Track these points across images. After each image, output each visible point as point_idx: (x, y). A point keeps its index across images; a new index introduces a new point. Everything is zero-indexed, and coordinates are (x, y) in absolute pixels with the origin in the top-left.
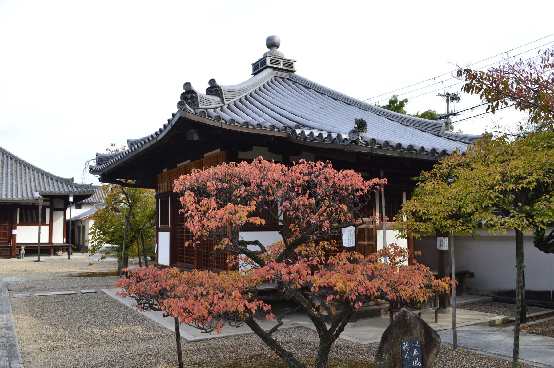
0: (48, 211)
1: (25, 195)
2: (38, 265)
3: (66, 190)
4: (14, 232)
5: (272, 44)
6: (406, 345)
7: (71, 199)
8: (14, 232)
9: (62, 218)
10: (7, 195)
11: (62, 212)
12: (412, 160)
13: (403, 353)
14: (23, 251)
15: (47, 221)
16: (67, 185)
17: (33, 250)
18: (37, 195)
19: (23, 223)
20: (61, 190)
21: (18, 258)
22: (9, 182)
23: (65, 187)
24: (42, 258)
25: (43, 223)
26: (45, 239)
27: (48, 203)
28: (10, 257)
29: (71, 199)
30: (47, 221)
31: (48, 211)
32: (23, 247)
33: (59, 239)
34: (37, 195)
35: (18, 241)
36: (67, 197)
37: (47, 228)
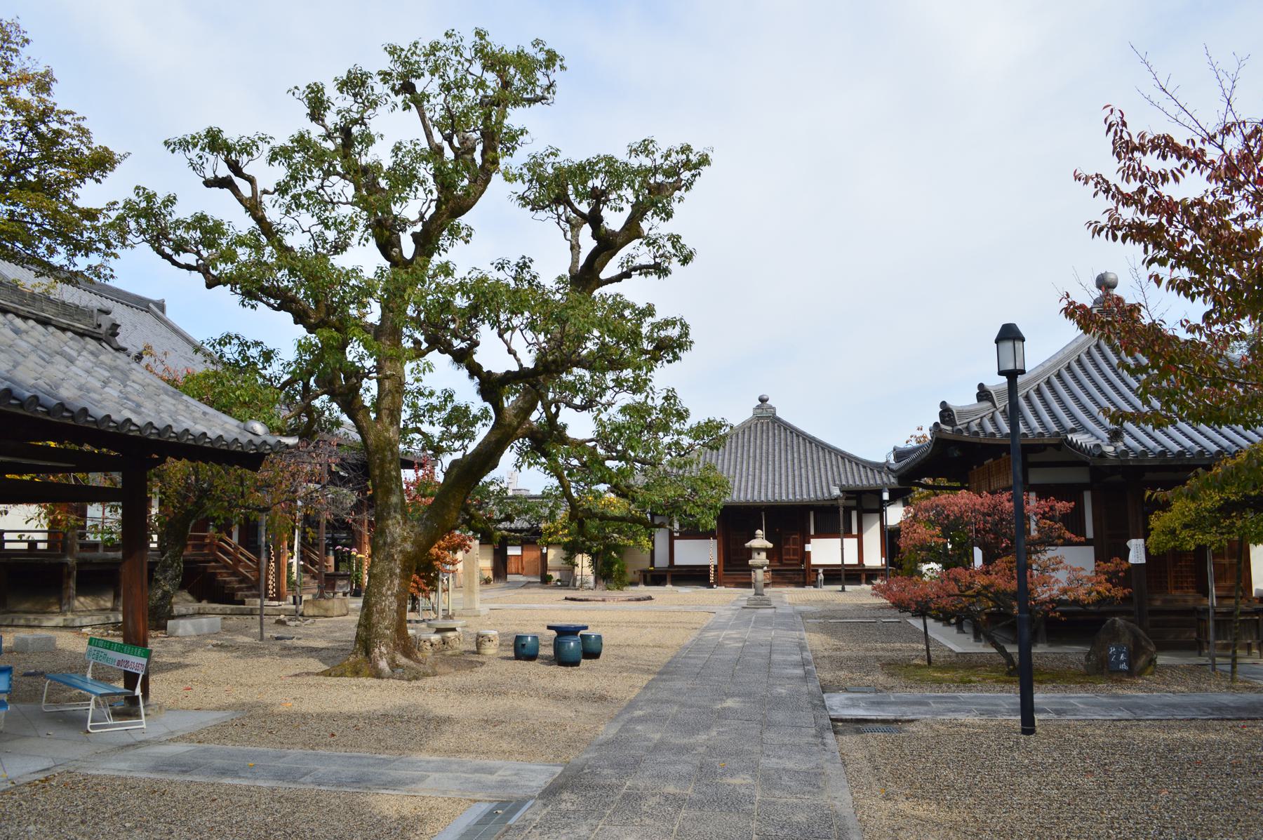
0: (854, 515)
1: (819, 493)
2: (842, 595)
3: (879, 482)
4: (808, 548)
5: (763, 400)
6: (1113, 650)
7: (886, 496)
8: (808, 548)
9: (878, 524)
10: (809, 495)
11: (877, 516)
12: (972, 445)
13: (1111, 656)
14: (821, 577)
15: (855, 531)
16: (880, 472)
17: (838, 575)
18: (836, 492)
19: (819, 535)
20: (872, 482)
21: (816, 586)
22: (797, 473)
23: (877, 477)
24: (848, 588)
25: (848, 533)
26: (851, 559)
27: (853, 503)
28: (803, 584)
29: (886, 496)
30: (855, 531)
31: (854, 515)
32: (821, 571)
33: (874, 558)
34: (836, 492)
35: (814, 561)
36: (879, 493)
37: (855, 540)
